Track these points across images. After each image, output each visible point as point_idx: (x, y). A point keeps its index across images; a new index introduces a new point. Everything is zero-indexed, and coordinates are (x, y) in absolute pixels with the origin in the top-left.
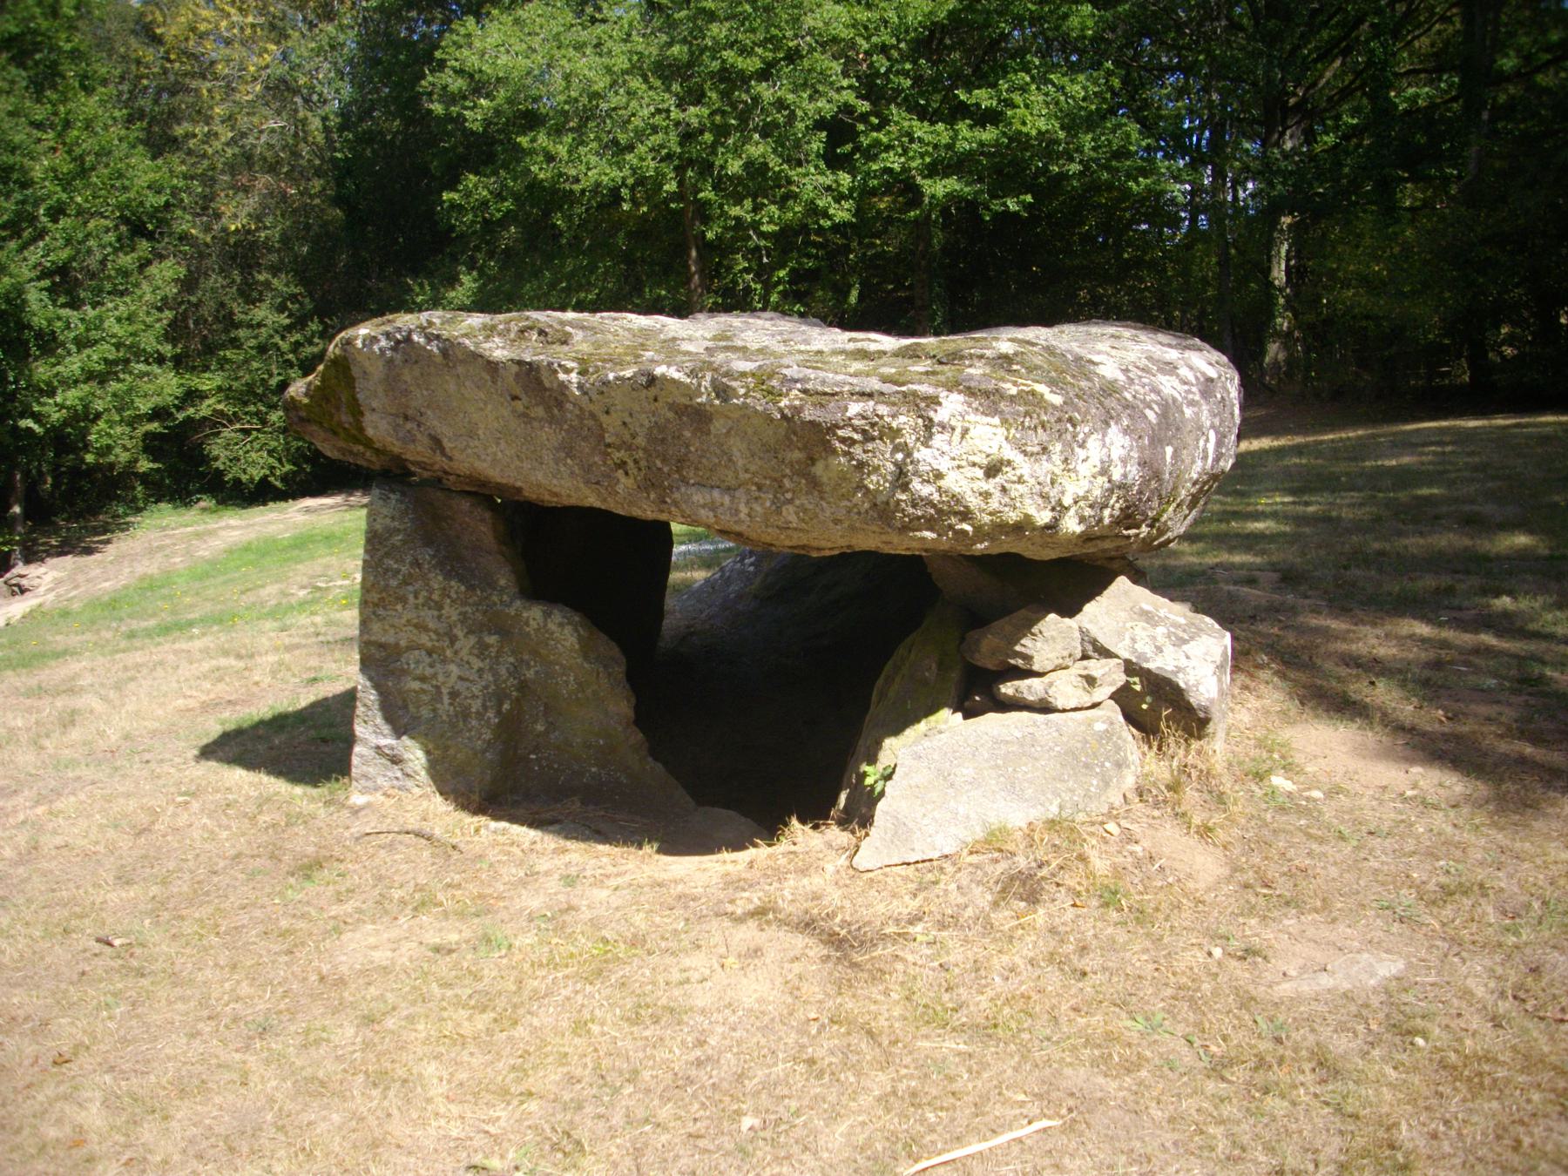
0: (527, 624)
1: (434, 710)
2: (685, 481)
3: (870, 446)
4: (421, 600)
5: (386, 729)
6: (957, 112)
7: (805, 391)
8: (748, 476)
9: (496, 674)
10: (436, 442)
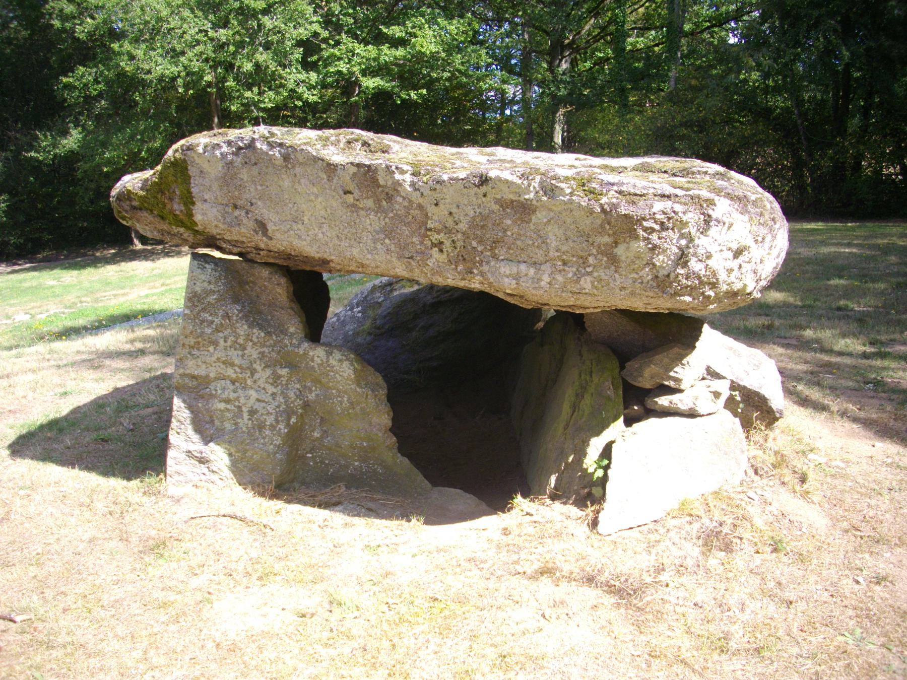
0: (313, 361)
1: (236, 424)
2: (494, 256)
3: (664, 234)
4: (229, 344)
5: (196, 437)
6: (379, 39)
7: (620, 192)
8: (557, 254)
9: (285, 396)
10: (262, 226)
